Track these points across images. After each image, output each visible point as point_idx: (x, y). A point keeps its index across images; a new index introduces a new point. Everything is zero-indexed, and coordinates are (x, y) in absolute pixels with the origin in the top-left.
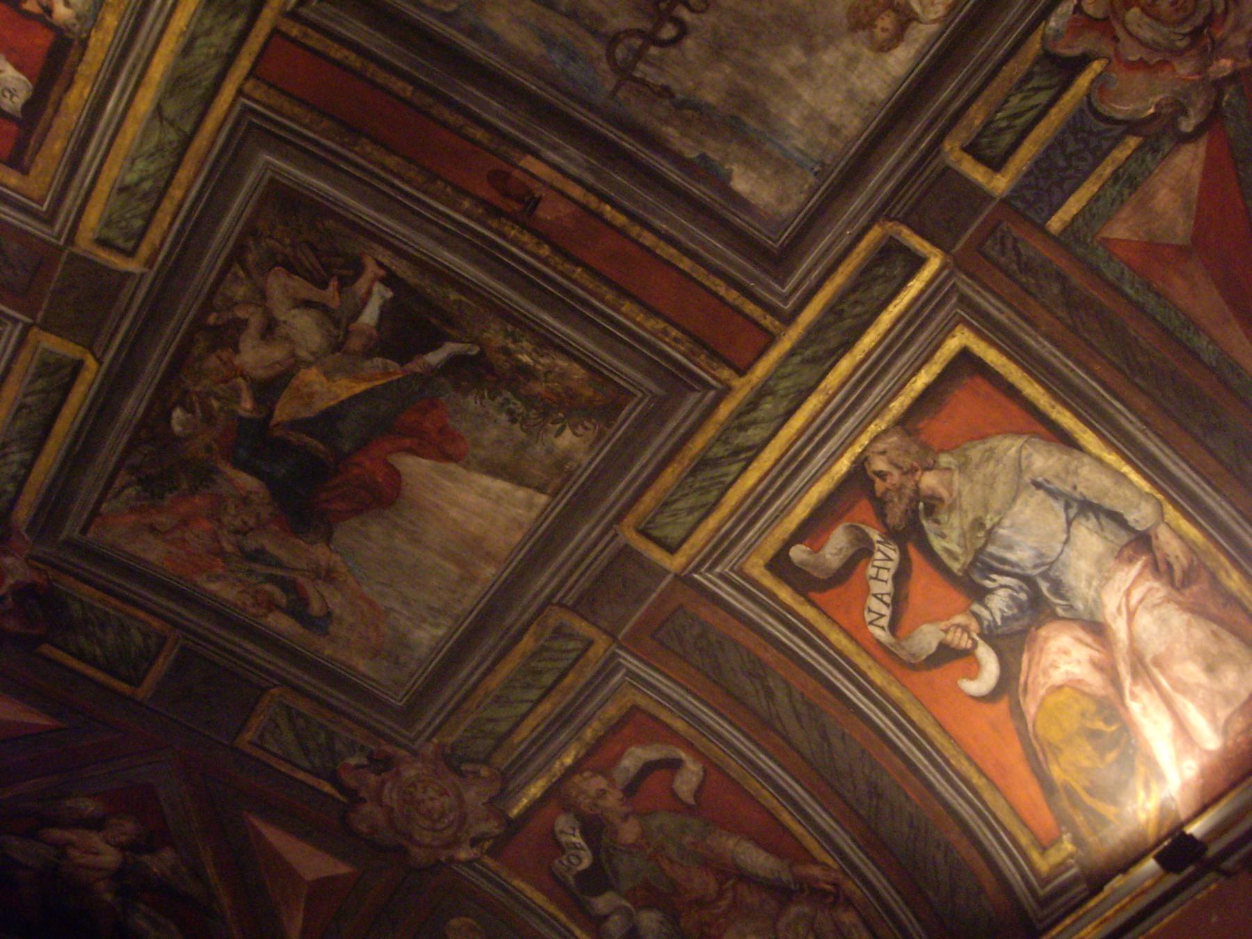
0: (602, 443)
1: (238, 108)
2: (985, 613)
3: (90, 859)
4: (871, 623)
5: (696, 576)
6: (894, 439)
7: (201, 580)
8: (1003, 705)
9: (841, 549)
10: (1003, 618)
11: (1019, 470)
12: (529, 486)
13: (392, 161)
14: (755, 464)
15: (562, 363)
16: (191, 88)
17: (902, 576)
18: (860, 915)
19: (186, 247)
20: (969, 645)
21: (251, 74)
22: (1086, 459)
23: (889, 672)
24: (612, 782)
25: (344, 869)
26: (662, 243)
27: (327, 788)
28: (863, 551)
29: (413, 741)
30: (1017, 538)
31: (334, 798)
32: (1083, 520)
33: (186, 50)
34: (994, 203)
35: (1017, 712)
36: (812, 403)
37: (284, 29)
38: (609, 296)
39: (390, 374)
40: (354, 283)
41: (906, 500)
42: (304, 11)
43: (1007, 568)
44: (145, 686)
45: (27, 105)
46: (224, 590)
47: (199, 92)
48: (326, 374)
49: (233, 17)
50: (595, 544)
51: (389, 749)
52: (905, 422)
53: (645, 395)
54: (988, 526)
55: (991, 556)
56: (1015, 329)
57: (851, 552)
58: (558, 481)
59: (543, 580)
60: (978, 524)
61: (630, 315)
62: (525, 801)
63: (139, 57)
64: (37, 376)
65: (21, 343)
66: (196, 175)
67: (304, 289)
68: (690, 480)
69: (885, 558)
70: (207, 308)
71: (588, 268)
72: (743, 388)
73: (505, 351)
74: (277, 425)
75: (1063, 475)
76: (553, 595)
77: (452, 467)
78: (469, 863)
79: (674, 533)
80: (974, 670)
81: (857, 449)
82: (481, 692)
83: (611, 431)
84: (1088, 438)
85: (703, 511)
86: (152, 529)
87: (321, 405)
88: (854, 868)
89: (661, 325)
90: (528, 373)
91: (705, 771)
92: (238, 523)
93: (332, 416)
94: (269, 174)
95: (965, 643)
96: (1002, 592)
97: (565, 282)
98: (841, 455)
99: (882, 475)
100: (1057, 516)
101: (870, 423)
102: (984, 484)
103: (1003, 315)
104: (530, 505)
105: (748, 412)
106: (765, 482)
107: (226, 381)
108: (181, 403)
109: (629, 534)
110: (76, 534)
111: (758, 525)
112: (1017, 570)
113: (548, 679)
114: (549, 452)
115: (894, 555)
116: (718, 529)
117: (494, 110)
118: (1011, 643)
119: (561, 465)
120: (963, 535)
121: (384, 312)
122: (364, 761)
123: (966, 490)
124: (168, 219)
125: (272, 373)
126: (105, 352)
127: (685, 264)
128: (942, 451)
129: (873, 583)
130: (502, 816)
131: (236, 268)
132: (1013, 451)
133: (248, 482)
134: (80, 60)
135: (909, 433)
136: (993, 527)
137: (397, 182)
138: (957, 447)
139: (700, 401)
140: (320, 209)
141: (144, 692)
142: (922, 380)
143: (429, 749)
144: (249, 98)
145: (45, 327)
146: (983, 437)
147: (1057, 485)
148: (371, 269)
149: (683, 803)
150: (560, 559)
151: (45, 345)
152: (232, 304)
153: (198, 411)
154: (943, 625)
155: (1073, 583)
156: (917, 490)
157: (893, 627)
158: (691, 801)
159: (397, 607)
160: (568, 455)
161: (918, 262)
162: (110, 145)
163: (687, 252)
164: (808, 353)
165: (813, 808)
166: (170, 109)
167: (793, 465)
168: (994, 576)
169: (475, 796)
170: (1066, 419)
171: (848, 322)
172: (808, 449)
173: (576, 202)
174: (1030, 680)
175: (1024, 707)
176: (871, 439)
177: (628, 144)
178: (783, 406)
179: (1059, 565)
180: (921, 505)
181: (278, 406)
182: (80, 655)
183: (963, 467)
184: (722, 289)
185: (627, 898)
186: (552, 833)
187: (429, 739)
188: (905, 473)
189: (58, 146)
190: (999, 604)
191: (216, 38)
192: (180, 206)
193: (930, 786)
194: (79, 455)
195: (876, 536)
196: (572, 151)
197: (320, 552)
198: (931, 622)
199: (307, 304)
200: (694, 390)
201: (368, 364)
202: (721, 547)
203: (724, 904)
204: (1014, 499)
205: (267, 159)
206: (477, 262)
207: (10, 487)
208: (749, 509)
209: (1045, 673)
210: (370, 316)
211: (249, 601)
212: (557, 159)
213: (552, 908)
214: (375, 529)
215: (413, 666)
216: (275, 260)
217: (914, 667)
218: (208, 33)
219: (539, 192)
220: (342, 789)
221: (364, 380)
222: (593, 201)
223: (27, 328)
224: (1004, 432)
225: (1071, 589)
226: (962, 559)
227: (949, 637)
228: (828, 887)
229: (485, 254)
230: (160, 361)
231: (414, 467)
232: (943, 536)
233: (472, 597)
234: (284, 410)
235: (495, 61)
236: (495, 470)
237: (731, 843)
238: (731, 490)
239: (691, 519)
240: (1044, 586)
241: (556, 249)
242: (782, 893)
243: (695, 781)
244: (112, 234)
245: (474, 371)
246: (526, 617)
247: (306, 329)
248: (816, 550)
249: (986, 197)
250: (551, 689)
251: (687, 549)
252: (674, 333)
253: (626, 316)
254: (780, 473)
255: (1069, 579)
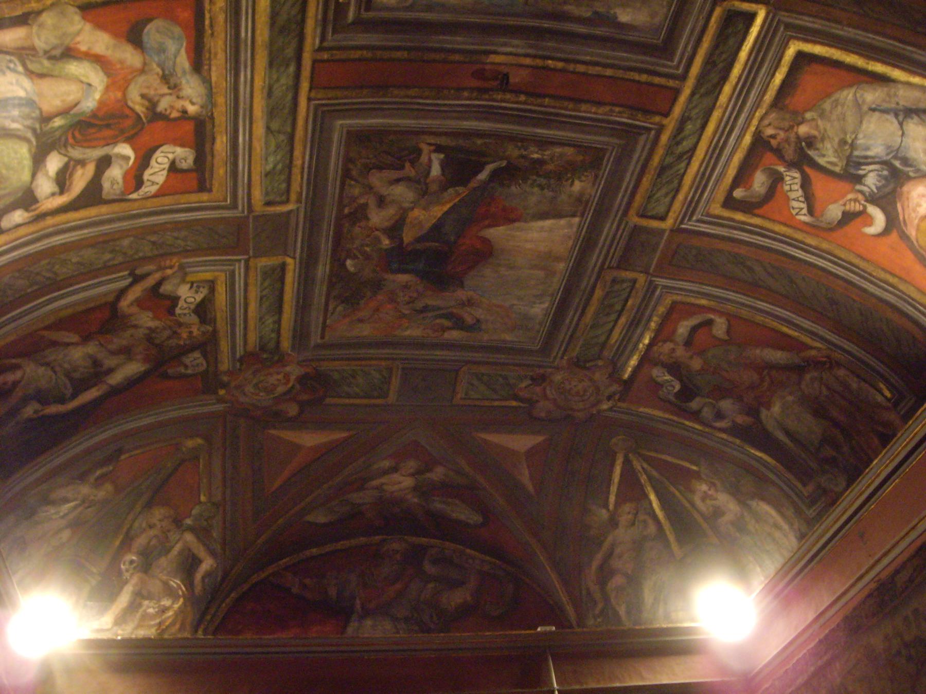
0: (598, 181)
1: (312, 107)
2: (865, 189)
3: (396, 487)
4: (797, 214)
5: (683, 226)
6: (773, 115)
7: (398, 332)
8: (894, 236)
9: (763, 183)
10: (877, 188)
11: (858, 105)
12: (567, 216)
13: (412, 92)
14: (694, 158)
15: (558, 150)
16: (282, 111)
17: (806, 184)
18: (848, 369)
19: (315, 186)
20: (861, 208)
21: (311, 89)
22: (900, 86)
23: (818, 236)
24: (676, 343)
25: (540, 439)
26: (590, 68)
27: (514, 403)
28: (777, 180)
29: (553, 362)
30: (871, 142)
31: (520, 407)
32: (910, 120)
33: (270, 94)
34: (667, 234)
35: (904, 237)
36: (716, 115)
37: (318, 58)
38: (571, 106)
39: (459, 194)
40: (419, 159)
41: (793, 145)
42: (325, 44)
43: (869, 160)
44: (391, 393)
45: (196, 161)
46: (413, 332)
47: (286, 111)
48: (424, 209)
49: (287, 66)
50: (615, 235)
51: (542, 371)
52: (777, 103)
53: (614, 148)
54: (850, 141)
55: (857, 157)
56: (827, 29)
57: (770, 181)
58: (581, 208)
59: (595, 257)
60: (843, 142)
61: (587, 111)
62: (630, 369)
63: (245, 110)
64: (264, 280)
65: (247, 268)
66: (305, 147)
67: (394, 174)
68: (659, 180)
69: (792, 180)
70: (341, 205)
71: (551, 97)
72: (671, 123)
73: (523, 157)
74: (407, 245)
75: (888, 99)
76: (603, 263)
77: (517, 224)
78: (611, 409)
79: (661, 209)
80: (870, 221)
81: (752, 128)
82: (582, 326)
83: (602, 172)
84: (897, 74)
85: (673, 193)
86: (361, 321)
87: (428, 225)
88: (835, 345)
89: (608, 108)
90: (541, 162)
91: (729, 321)
92: (406, 298)
93: (438, 227)
94: (345, 130)
95: (858, 208)
96: (871, 174)
97: (543, 109)
98: (744, 135)
99: (773, 137)
100: (892, 123)
101: (755, 111)
102: (839, 120)
103: (817, 24)
104: (570, 226)
105: (679, 134)
106: (704, 165)
107: (368, 236)
108: (348, 256)
109: (634, 220)
110: (319, 341)
111: (709, 188)
112: (877, 160)
113: (618, 307)
114: (570, 196)
115: (797, 175)
116: (686, 198)
117: (460, 41)
118: (888, 199)
119: (581, 201)
120: (836, 151)
121: (444, 165)
122: (530, 382)
123: (828, 126)
124: (299, 176)
125: (392, 222)
126: (295, 253)
127: (609, 72)
128: (806, 111)
129: (789, 194)
130: (620, 381)
131: (348, 181)
132: (850, 96)
133: (403, 278)
134: (214, 126)
135: (782, 109)
136: (853, 141)
137: (421, 101)
138: (814, 105)
139: (647, 139)
140: (380, 134)
141: (392, 397)
142: (779, 78)
143: (564, 362)
144: (315, 100)
145: (255, 257)
146: (828, 95)
147: (885, 106)
148: (425, 149)
149: (719, 339)
150: (600, 245)
151: (259, 265)
152: (354, 199)
153: (359, 256)
154: (841, 202)
155: (916, 157)
156: (798, 137)
157: (811, 212)
158: (726, 338)
159: (515, 302)
160: (581, 194)
161: (752, 17)
162: (250, 156)
163: (605, 66)
164: (702, 90)
165: (799, 320)
166: (275, 126)
167: (716, 151)
168: (863, 167)
169: (599, 376)
170: (879, 68)
171: (721, 66)
172: (723, 139)
173: (527, 66)
174: (906, 217)
175: (908, 233)
176: (760, 119)
177: (546, 24)
178: (699, 123)
179: (902, 148)
180: (803, 144)
181: (404, 235)
182: (349, 396)
183: (822, 115)
184: (636, 76)
185: (708, 397)
186: (652, 379)
187: (562, 358)
188: (787, 131)
189: (222, 172)
190: (872, 181)
191: (283, 81)
192: (303, 168)
193: (865, 291)
194: (303, 306)
195: (782, 169)
196: (516, 42)
197: (461, 294)
198: (835, 201)
199: (398, 181)
200: (640, 134)
201: (445, 194)
202: (691, 207)
203: (766, 384)
204: (861, 122)
205: (341, 124)
206: (487, 119)
207: (273, 335)
208: (700, 182)
209: (914, 210)
210: (436, 170)
211: (430, 332)
212: (509, 49)
213: (667, 416)
214: (487, 271)
215: (537, 327)
216: (367, 169)
217: (831, 230)
218: (278, 80)
219: (505, 70)
220: (522, 400)
221: (447, 202)
222: (539, 62)
223: (247, 261)
224: (842, 88)
225: (915, 160)
226: (840, 164)
227: (847, 207)
228: (824, 359)
229: (487, 113)
230: (327, 240)
231: (496, 233)
232: (824, 156)
233: (557, 283)
234: (408, 236)
235: (448, 17)
236: (543, 216)
237: (758, 351)
238: (685, 177)
239: (668, 199)
240: (897, 164)
241: (527, 94)
242: (799, 369)
243: (724, 327)
244: (271, 197)
245: (509, 173)
246: (593, 280)
247: (402, 193)
248: (748, 186)
249: (663, 231)
250: (623, 309)
251: (672, 216)
252: (617, 109)
253: (584, 112)
254: (711, 158)
255: (911, 154)
